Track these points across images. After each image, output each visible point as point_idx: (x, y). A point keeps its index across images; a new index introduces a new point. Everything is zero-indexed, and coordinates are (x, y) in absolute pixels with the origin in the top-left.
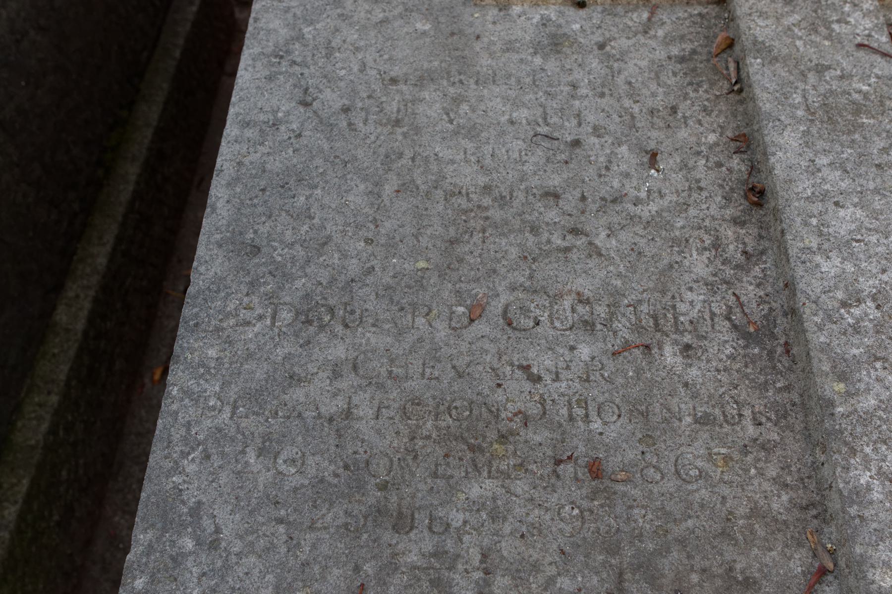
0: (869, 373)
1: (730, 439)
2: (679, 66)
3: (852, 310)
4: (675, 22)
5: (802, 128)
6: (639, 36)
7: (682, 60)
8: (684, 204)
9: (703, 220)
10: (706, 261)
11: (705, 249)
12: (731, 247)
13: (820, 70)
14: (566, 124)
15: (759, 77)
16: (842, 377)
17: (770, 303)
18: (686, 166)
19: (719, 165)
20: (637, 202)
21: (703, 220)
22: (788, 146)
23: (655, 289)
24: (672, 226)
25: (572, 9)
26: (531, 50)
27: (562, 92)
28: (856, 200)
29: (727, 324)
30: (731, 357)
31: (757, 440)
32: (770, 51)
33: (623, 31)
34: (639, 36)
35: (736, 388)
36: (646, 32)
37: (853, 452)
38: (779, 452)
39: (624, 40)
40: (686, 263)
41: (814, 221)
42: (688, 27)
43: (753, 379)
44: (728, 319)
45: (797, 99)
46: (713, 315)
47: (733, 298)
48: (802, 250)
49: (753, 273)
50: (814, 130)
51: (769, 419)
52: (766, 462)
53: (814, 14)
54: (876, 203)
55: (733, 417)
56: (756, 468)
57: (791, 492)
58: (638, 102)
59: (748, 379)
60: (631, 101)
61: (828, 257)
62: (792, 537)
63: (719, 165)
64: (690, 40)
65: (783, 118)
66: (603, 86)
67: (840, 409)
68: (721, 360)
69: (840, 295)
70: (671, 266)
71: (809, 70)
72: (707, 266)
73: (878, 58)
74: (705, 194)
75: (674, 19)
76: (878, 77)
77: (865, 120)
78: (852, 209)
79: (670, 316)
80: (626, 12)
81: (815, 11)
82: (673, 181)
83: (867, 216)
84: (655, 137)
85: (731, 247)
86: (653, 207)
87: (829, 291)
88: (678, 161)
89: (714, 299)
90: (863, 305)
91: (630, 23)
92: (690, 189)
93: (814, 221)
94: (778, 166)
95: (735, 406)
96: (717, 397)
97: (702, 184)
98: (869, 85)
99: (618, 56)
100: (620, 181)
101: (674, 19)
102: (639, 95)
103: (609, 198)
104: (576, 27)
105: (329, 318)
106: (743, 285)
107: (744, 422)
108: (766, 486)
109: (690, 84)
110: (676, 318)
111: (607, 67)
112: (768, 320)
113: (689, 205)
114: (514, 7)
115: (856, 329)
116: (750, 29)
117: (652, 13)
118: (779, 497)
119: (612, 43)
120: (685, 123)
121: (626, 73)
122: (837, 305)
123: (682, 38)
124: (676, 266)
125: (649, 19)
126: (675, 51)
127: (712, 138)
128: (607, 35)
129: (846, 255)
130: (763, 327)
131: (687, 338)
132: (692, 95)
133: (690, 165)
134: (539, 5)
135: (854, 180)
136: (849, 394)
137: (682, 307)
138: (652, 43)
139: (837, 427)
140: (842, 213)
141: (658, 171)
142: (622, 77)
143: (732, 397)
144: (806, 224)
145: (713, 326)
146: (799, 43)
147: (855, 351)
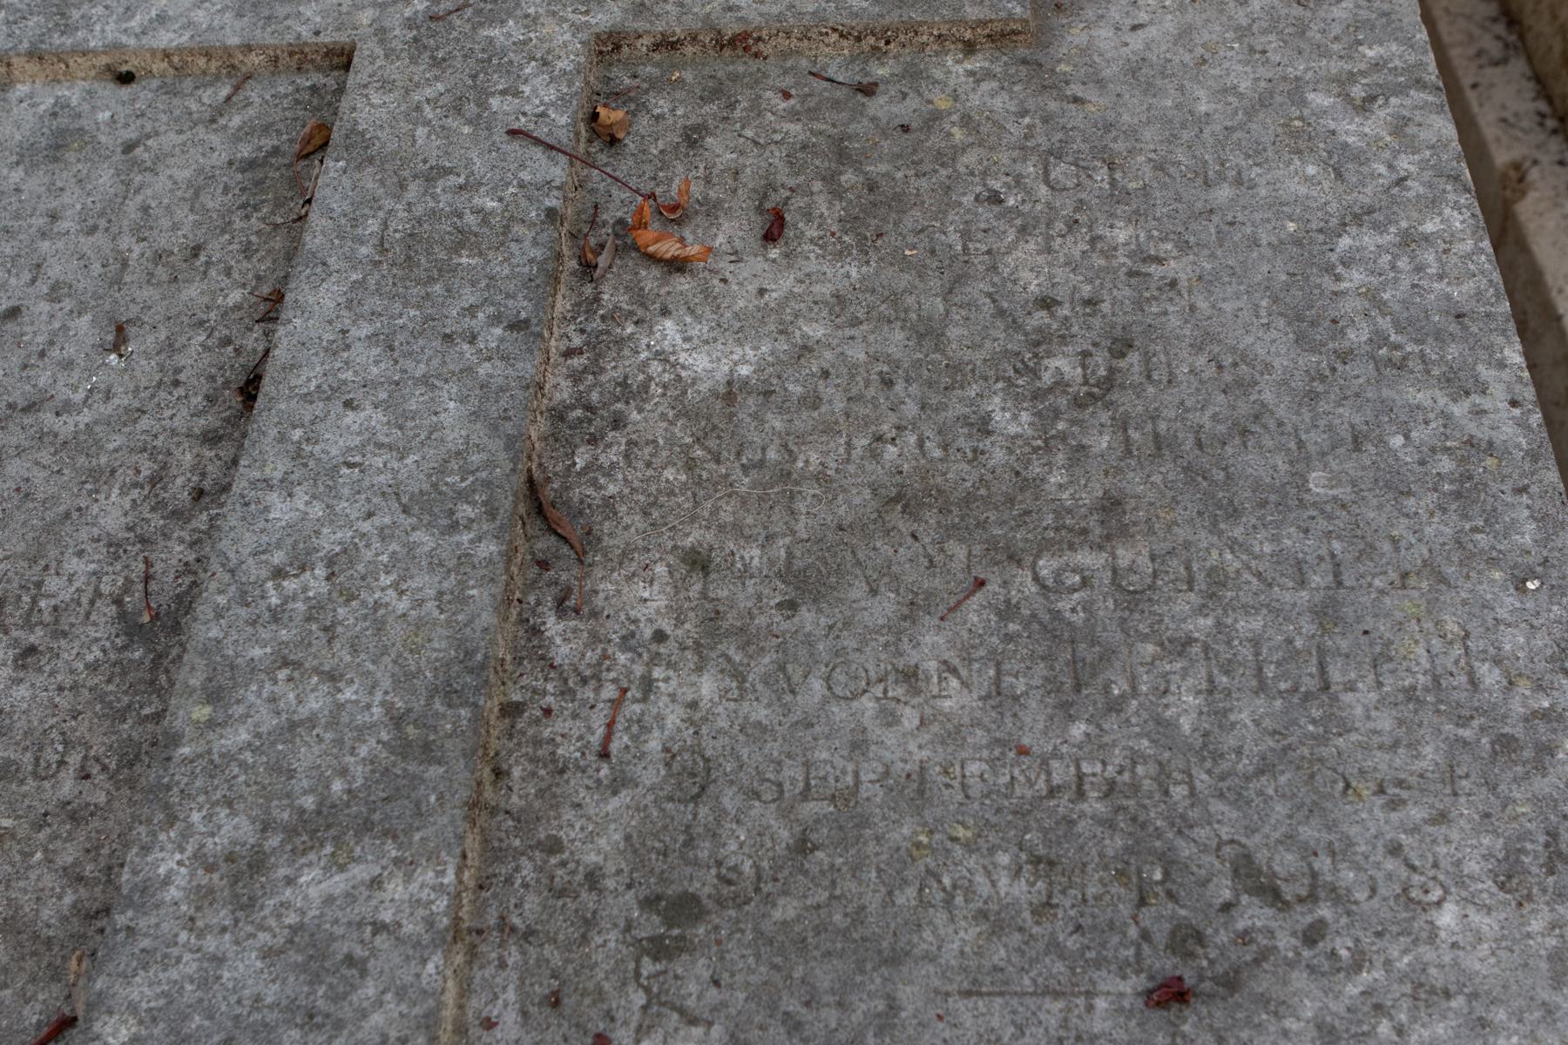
0: (261, 687)
1: (27, 802)
2: (239, 176)
3: (285, 583)
4: (267, 102)
5: (354, 277)
6: (201, 129)
7: (250, 165)
8: (138, 410)
9: (155, 436)
10: (128, 506)
11: (135, 485)
12: (179, 481)
13: (433, 175)
14: (13, 281)
15: (328, 192)
16: (214, 696)
17: (196, 573)
18: (170, 345)
19: (227, 341)
20: (66, 408)
21: (155, 436)
22: (316, 308)
23: (23, 555)
24: (102, 447)
25: (111, 86)
26: (14, 158)
27: (30, 226)
28: (383, 395)
29: (112, 610)
30: (93, 667)
31: (69, 803)
32: (367, 147)
33: (177, 120)
34: (201, 129)
35: (75, 718)
36: (213, 121)
37: (172, 820)
38: (96, 823)
39: (172, 135)
40: (95, 509)
41: (297, 434)
42: (284, 109)
43: (111, 702)
44: (118, 602)
45: (373, 226)
46: (98, 594)
47: (142, 567)
48: (253, 484)
49: (194, 524)
50: (372, 281)
51: (105, 768)
52: (66, 841)
53: (470, 82)
54: (413, 400)
55: (49, 766)
56: (46, 851)
57: (82, 890)
58: (144, 239)
59: (102, 702)
60: (134, 240)
61: (290, 495)
62: (49, 965)
63: (227, 341)
64: (277, 131)
65: (331, 261)
66: (102, 214)
67: (185, 750)
68: (72, 672)
69: (278, 558)
70: (67, 515)
71: (415, 177)
72: (126, 514)
73: (538, 153)
74: (181, 391)
75: (268, 97)
76: (521, 185)
77: (464, 260)
78: (369, 411)
79: (27, 599)
80: (197, 88)
81: (474, 77)
82: (138, 374)
83: (388, 423)
84: (141, 295)
85: (179, 481)
86: (86, 417)
87: (264, 552)
88: (163, 337)
89: (110, 569)
90: (308, 573)
91: (194, 107)
92: (160, 383)
93: (297, 434)
94: (285, 341)
95: (60, 748)
96: (37, 734)
97: (182, 377)
98: (501, 200)
99: (149, 164)
100: (54, 375)
101: (268, 97)
102: (151, 228)
103: (21, 403)
104: (103, 116)
105: (1044, 572)
106: (169, 544)
107: (62, 774)
108: (49, 880)
109: (243, 206)
110: (34, 601)
111: (122, 182)
112: (181, 602)
113: (144, 412)
114: (19, 86)
115: (276, 616)
116: (354, 109)
117: (237, 88)
118: (60, 898)
119: (150, 143)
120: (205, 273)
121: (149, 192)
122: (264, 573)
123: (266, 129)
124: (75, 515)
125: (228, 98)
126: (245, 151)
127: (236, 296)
128: (148, 129)
129: (322, 488)
130: (168, 614)
131: (37, 637)
132: (238, 224)
133: (177, 345)
134: (59, 82)
135: (396, 362)
136: (211, 724)
137: (52, 583)
138: (215, 139)
139: (166, 780)
140: (350, 417)
141: (121, 356)
142: (139, 198)
143: (63, 734)
144: (282, 438)
145: (88, 615)
146: (421, 132)
147: (257, 652)
